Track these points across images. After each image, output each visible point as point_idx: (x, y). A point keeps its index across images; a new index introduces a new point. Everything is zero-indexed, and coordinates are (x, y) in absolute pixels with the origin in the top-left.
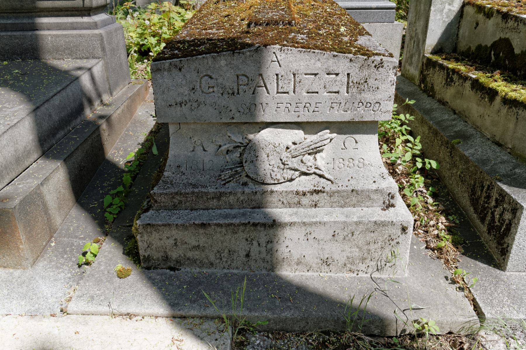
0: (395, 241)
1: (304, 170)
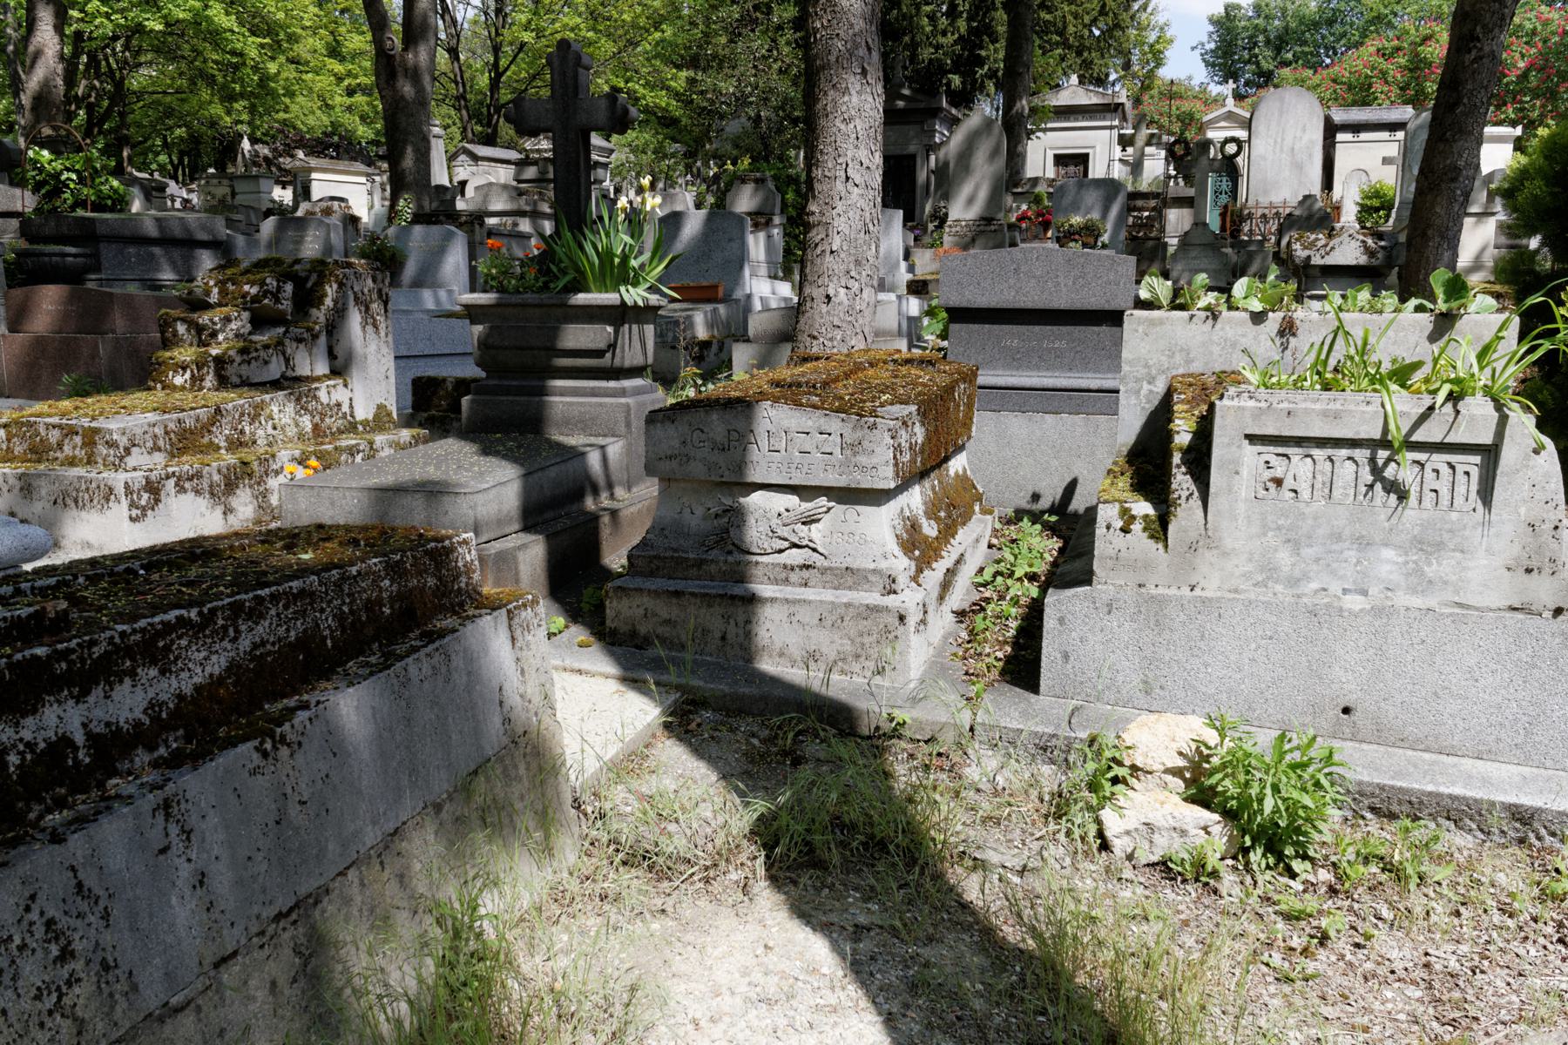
0: (893, 634)
1: (796, 540)
